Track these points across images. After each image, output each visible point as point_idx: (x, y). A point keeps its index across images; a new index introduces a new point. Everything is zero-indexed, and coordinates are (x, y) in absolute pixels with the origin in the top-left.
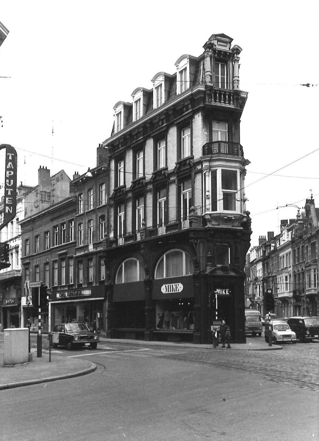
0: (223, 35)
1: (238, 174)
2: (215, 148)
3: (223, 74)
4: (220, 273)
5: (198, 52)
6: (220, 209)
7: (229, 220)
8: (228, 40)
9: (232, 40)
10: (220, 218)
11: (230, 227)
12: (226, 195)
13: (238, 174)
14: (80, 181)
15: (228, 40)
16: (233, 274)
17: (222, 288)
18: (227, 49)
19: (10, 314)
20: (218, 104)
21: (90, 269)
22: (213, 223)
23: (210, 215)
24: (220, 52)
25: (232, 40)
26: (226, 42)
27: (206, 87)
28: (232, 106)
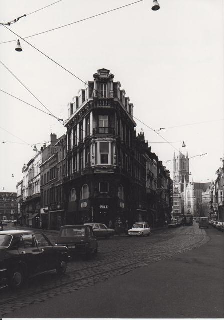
0: (104, 70)
1: (110, 145)
2: (102, 131)
3: (105, 89)
4: (101, 197)
5: (92, 80)
6: (99, 164)
7: (104, 169)
8: (107, 72)
9: (109, 71)
10: (99, 168)
11: (107, 172)
12: (102, 156)
13: (110, 145)
14: (59, 207)
15: (107, 72)
16: (109, 197)
17: (103, 205)
18: (106, 76)
19: (111, 141)
20: (101, 107)
21: (40, 192)
22: (98, 170)
23: (94, 167)
24: (102, 79)
25: (109, 71)
26: (106, 73)
27: (94, 98)
28: (109, 107)
